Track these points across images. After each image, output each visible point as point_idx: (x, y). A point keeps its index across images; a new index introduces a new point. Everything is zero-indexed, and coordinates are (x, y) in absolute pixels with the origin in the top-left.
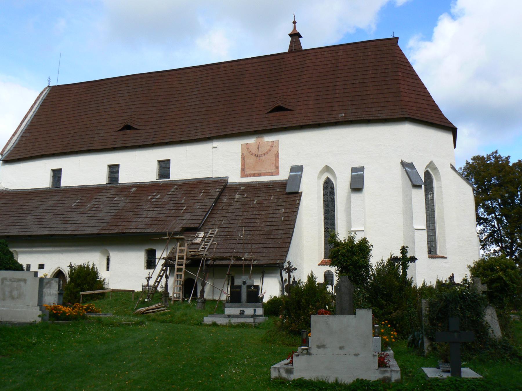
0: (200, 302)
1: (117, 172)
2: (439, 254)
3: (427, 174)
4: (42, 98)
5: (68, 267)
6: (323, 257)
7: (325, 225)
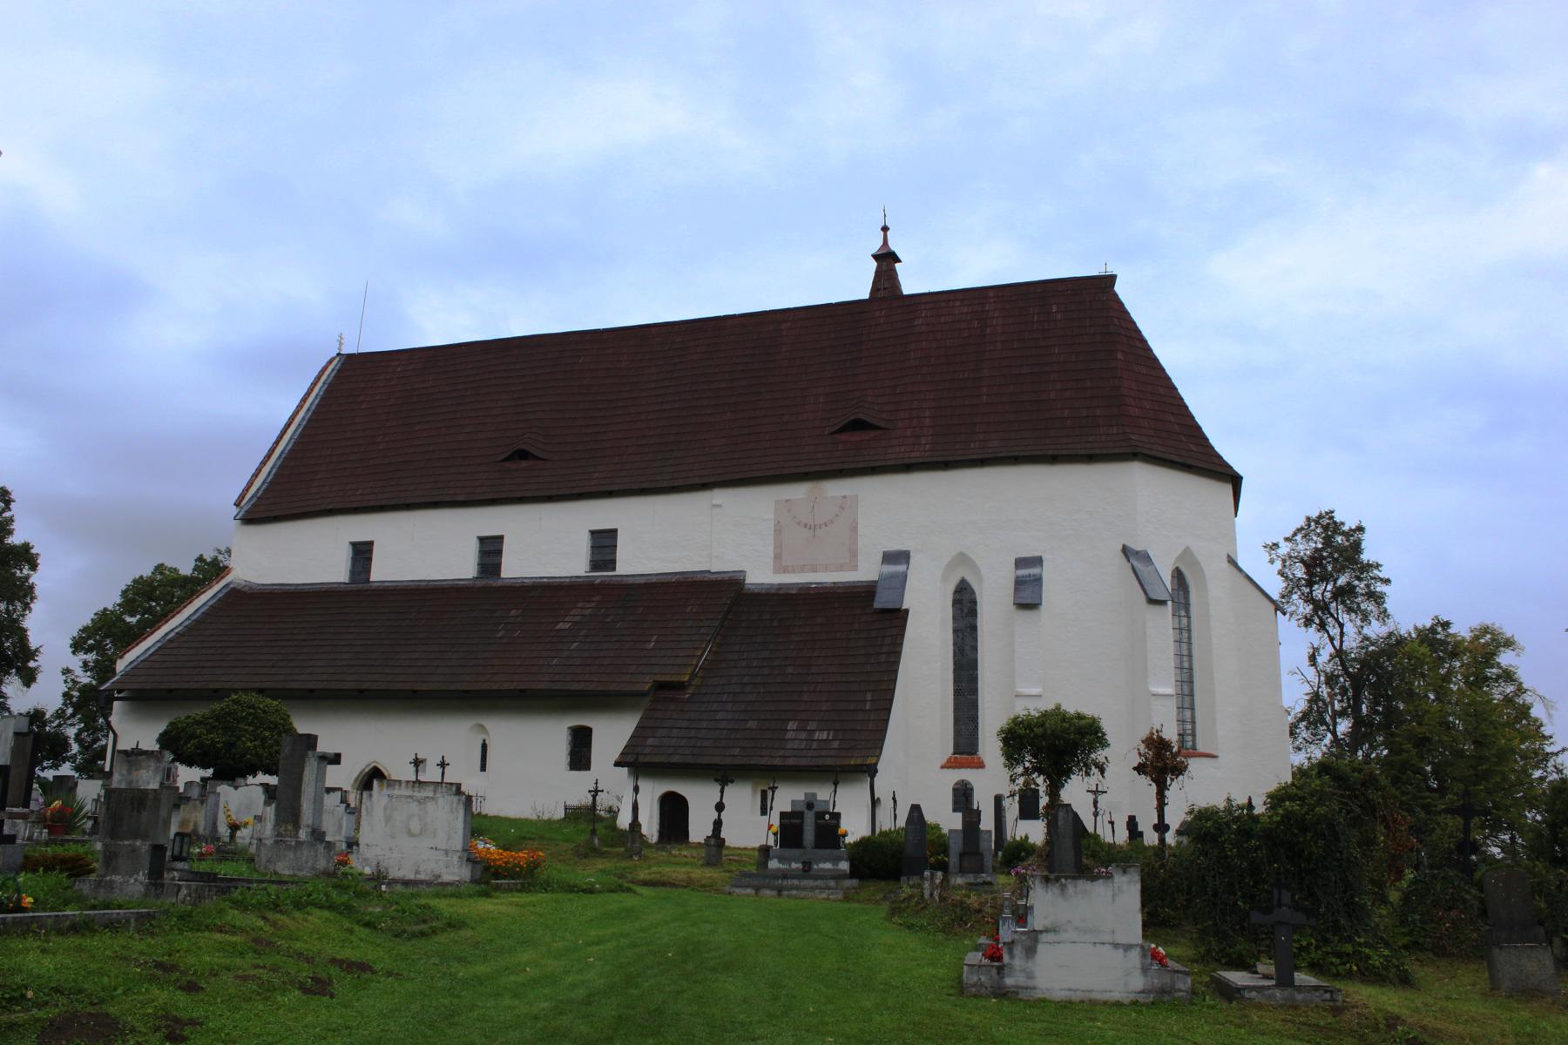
0: (714, 846)
1: (499, 553)
2: (1201, 748)
3: (1178, 576)
4: (326, 380)
5: (411, 763)
6: (951, 750)
7: (955, 681)
